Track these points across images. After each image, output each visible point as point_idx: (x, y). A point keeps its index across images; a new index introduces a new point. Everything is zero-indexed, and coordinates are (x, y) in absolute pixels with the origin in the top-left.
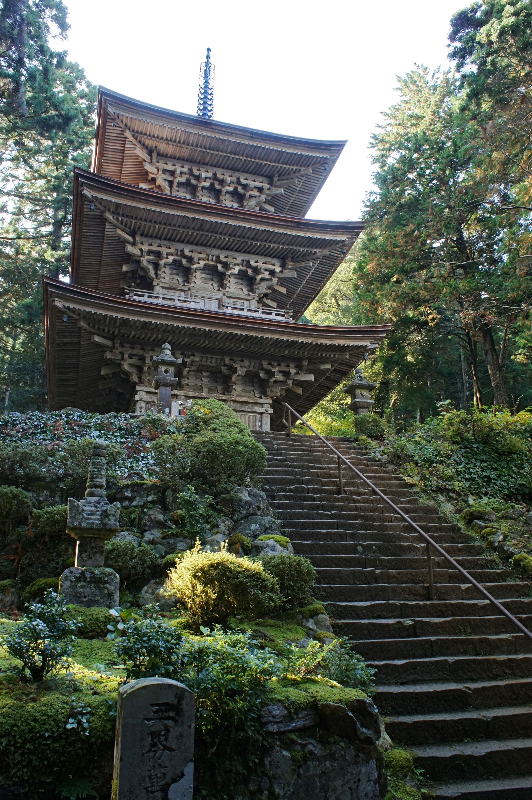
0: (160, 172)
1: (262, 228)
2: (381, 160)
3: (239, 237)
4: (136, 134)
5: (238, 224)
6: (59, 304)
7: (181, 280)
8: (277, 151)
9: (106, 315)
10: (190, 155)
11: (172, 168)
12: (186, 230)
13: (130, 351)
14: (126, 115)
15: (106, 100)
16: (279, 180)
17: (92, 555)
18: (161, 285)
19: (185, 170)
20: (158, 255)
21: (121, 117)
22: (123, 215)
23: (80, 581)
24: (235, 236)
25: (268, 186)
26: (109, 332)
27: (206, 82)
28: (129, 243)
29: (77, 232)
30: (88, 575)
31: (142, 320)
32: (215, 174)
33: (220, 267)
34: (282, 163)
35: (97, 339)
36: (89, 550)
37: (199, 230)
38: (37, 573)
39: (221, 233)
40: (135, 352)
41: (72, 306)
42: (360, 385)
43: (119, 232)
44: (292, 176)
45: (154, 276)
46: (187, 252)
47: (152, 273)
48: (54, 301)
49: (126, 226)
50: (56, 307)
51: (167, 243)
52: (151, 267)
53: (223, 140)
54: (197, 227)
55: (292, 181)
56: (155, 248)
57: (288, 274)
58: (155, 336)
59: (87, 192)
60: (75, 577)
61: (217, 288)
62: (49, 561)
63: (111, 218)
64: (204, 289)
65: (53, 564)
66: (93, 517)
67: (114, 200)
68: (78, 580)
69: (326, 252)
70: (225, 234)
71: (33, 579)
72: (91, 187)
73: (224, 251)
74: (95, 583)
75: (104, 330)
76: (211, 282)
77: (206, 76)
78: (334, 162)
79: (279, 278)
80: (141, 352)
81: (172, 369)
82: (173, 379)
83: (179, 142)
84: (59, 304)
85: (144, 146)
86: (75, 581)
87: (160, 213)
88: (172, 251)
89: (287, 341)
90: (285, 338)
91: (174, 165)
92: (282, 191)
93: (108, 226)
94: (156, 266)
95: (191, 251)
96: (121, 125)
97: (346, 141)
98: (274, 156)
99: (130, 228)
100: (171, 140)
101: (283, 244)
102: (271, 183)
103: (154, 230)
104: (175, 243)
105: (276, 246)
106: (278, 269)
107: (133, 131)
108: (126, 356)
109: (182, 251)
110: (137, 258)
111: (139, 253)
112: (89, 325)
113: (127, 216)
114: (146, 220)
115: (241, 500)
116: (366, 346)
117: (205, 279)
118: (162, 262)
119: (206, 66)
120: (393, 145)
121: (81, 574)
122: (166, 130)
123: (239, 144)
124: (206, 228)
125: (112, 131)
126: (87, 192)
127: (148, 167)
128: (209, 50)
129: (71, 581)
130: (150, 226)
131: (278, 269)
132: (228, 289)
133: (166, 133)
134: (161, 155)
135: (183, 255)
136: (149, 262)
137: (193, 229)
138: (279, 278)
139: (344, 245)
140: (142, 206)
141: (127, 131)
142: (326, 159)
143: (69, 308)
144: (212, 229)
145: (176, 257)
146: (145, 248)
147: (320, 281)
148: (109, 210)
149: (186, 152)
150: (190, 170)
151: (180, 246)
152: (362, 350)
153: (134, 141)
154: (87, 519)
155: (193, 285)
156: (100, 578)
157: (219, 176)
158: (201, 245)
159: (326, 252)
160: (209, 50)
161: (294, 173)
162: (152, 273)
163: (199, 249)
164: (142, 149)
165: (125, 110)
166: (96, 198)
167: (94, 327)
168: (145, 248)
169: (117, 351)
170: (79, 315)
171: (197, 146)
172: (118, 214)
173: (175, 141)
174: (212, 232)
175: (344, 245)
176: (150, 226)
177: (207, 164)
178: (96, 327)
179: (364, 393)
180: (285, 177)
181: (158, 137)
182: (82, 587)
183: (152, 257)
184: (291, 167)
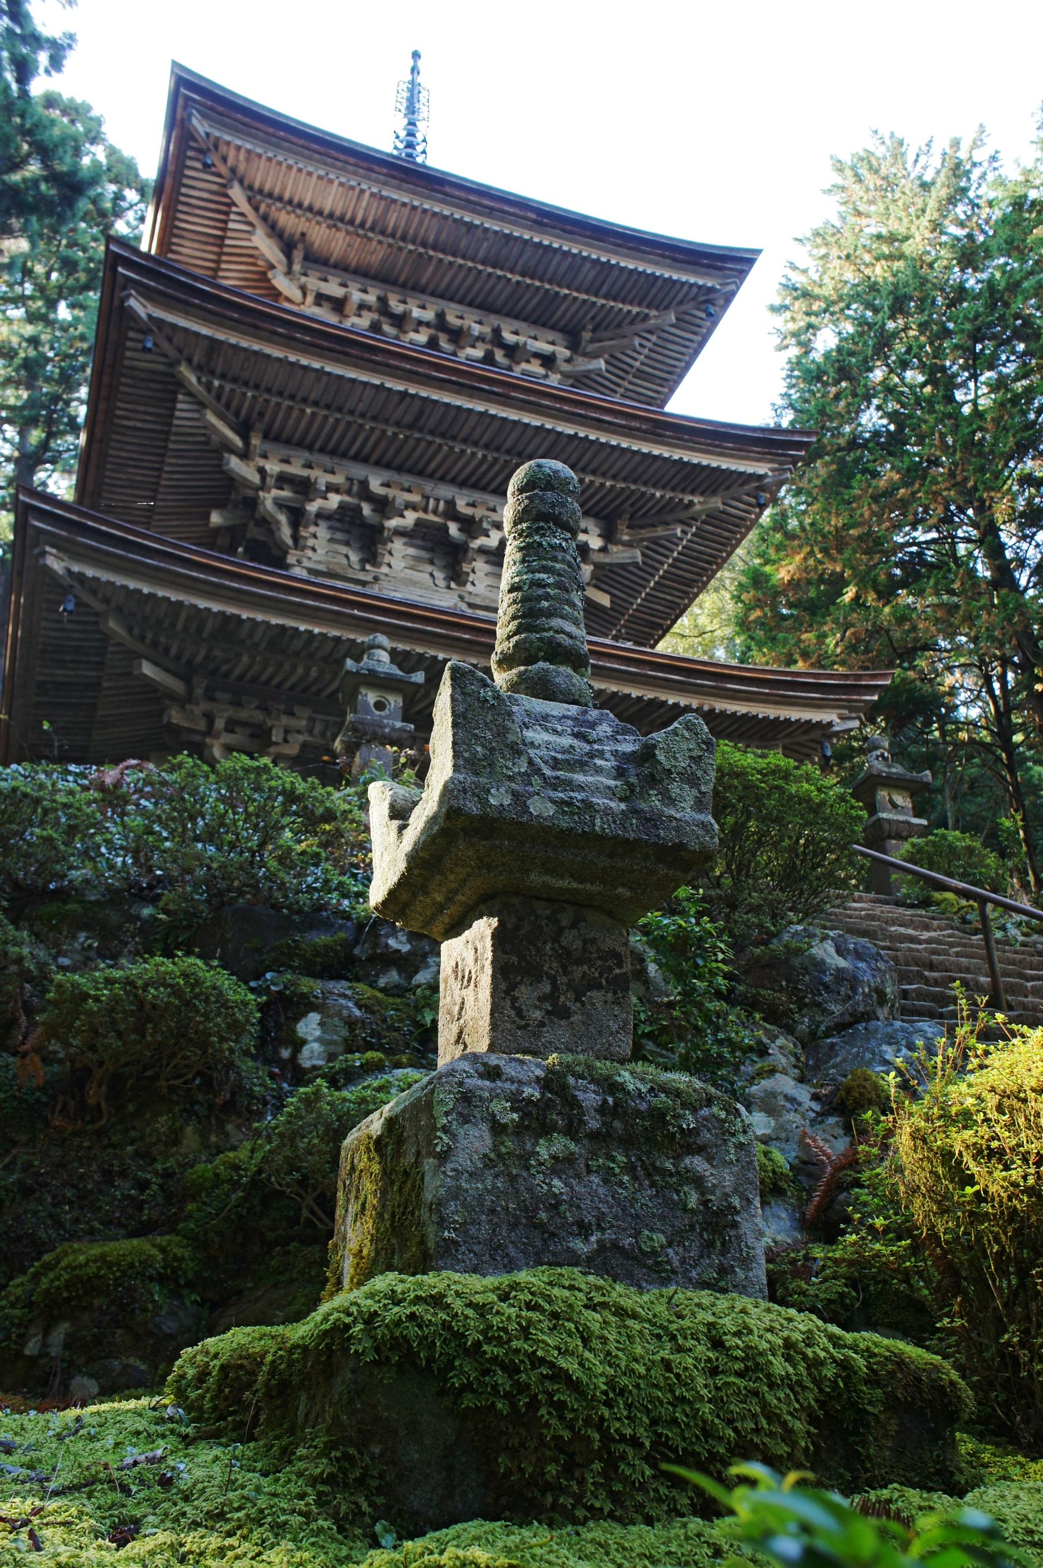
0: (310, 299)
1: (569, 430)
2: (803, 338)
3: (508, 452)
4: (256, 194)
5: (513, 415)
6: (56, 563)
7: (354, 558)
8: (597, 261)
9: (180, 603)
10: (384, 261)
11: (338, 292)
12: (381, 426)
13: (230, 712)
14: (238, 145)
15: (188, 99)
16: (592, 341)
17: (566, 999)
18: (306, 563)
19: (371, 298)
20: (305, 488)
21: (223, 149)
22: (223, 377)
23: (546, 1130)
24: (498, 449)
25: (567, 353)
26: (178, 657)
27: (412, 123)
28: (233, 451)
29: (101, 417)
30: (589, 1098)
31: (275, 621)
32: (441, 316)
33: (453, 529)
34: (605, 297)
35: (147, 669)
36: (551, 966)
37: (411, 427)
38: (58, 1224)
39: (465, 441)
40: (243, 714)
41: (90, 572)
42: (889, 777)
43: (211, 418)
44: (626, 329)
45: (290, 542)
46: (375, 485)
47: (286, 532)
48: (44, 553)
49: (228, 406)
50: (48, 571)
51: (326, 460)
52: (283, 518)
53: (470, 226)
54: (408, 419)
55: (625, 342)
56: (296, 469)
57: (619, 554)
58: (300, 670)
59: (138, 305)
60: (517, 1102)
61: (442, 583)
62: (108, 1176)
63: (194, 380)
64: (414, 583)
65: (124, 1188)
66: (580, 778)
67: (205, 331)
68: (535, 1120)
69: (716, 503)
70: (475, 444)
71: (40, 1248)
72: (147, 294)
73: (465, 491)
74: (627, 1142)
75: (167, 650)
76: (429, 568)
77: (411, 109)
78: (729, 298)
79: (598, 566)
80: (259, 716)
81: (395, 701)
82: (399, 724)
83: (362, 225)
84: (56, 563)
85: (275, 231)
86: (520, 1130)
87: (320, 372)
88: (338, 479)
89: (639, 699)
90: (635, 693)
91: (345, 285)
92: (601, 364)
93: (183, 406)
94: (297, 517)
95: (387, 485)
96: (223, 169)
97: (758, 252)
98: (588, 274)
99: (237, 414)
100: (342, 219)
101: (614, 477)
102: (574, 346)
103: (299, 420)
104: (345, 462)
105: (599, 481)
106: (595, 543)
107: (250, 188)
108: (220, 724)
109: (364, 484)
110: (250, 493)
111: (256, 479)
112: (130, 630)
113: (235, 380)
114: (280, 394)
115: (820, 965)
116: (830, 724)
117: (416, 558)
118: (312, 507)
119: (411, 91)
120: (834, 303)
121: (545, 1083)
122: (332, 193)
123: (508, 237)
124: (432, 423)
125: (199, 186)
126: (138, 305)
127: (280, 282)
128: (416, 55)
129: (497, 1129)
130: (290, 409)
131: (595, 543)
132: (469, 587)
133: (332, 199)
134: (317, 260)
135: (364, 492)
136: (279, 503)
137: (398, 424)
138: (598, 566)
139: (762, 488)
140: (277, 353)
141: (236, 185)
142: (711, 290)
143: (81, 578)
144: (443, 428)
145: (347, 499)
146: (273, 467)
147: (690, 583)
148: (189, 361)
149: (375, 252)
150: (383, 300)
151: (359, 471)
152: (816, 734)
153: (252, 216)
154: (555, 784)
155: (384, 569)
156: (658, 1116)
157: (451, 319)
158: (410, 471)
159: (716, 503)
160: (416, 55)
161: (632, 323)
162: (286, 532)
163: (406, 480)
164: (269, 236)
165: (234, 130)
166: (160, 323)
167: (142, 638)
168: (273, 467)
169: (198, 710)
170: (107, 601)
171: (403, 238)
172: (212, 373)
173: (351, 222)
174: (443, 435)
175: (762, 488)
176: (290, 409)
177: (423, 291)
178: (149, 636)
179: (899, 799)
180: (609, 334)
181: (310, 209)
182: (561, 1164)
183: (286, 493)
184: (627, 308)
